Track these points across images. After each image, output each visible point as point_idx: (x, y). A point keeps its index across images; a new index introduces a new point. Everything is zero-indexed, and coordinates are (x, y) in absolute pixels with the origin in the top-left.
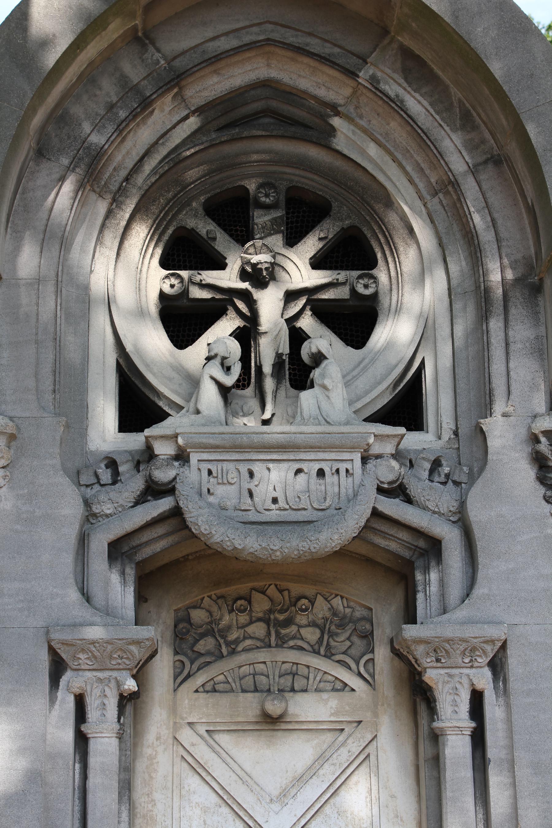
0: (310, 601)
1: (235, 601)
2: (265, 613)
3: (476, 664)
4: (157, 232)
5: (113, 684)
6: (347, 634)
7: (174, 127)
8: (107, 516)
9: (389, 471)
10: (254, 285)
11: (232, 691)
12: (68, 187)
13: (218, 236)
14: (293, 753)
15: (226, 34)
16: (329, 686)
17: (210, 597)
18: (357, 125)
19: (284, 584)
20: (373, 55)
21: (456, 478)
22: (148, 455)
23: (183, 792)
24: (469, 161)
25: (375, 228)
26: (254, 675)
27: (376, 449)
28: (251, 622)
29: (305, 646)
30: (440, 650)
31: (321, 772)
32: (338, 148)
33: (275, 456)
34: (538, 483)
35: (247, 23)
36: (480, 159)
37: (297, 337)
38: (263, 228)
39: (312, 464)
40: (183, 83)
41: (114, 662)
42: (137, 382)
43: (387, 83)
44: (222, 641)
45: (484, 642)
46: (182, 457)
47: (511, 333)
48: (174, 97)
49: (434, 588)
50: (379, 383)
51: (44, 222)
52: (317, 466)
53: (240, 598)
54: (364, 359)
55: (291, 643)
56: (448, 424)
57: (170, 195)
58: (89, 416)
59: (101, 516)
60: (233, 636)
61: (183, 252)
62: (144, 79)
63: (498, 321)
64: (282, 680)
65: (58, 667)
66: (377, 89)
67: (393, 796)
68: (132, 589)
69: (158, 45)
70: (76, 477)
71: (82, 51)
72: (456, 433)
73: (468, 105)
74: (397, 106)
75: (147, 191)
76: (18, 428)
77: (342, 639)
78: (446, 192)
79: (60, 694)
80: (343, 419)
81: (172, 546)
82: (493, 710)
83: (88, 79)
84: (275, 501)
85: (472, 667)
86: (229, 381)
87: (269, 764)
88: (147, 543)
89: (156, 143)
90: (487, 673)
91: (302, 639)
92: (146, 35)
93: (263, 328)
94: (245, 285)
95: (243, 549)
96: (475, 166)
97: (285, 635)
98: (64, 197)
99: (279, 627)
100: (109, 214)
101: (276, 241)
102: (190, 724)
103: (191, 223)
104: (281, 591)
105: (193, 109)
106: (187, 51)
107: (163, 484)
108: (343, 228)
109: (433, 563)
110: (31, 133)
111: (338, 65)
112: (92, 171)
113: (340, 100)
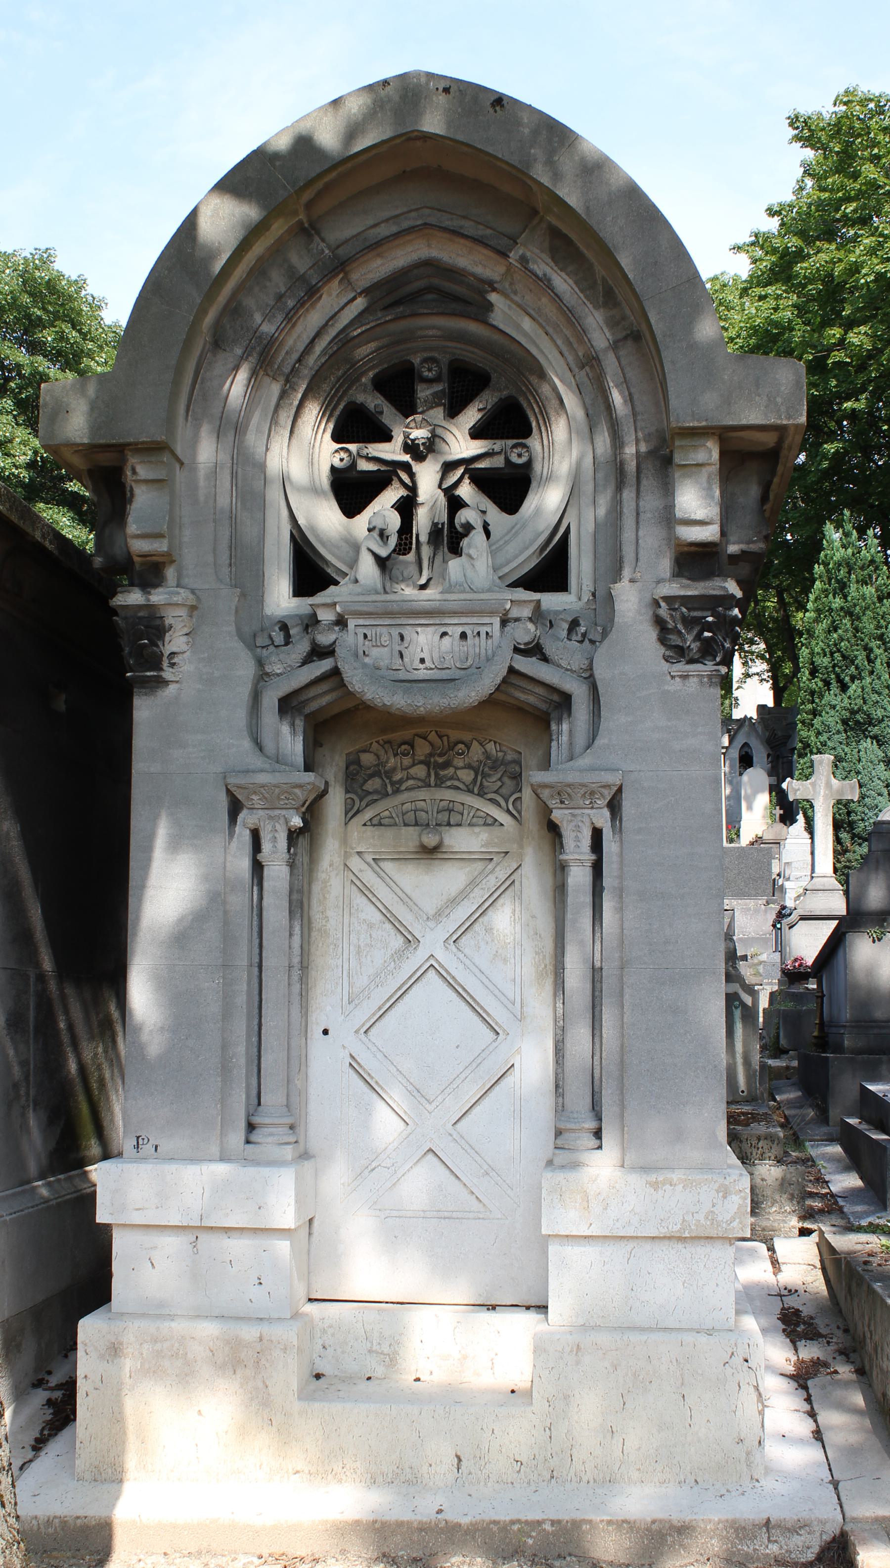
0: (466, 746)
1: (400, 746)
2: (426, 757)
3: (596, 806)
4: (327, 410)
5: (282, 821)
6: (499, 775)
7: (342, 308)
8: (278, 675)
9: (525, 633)
10: (413, 459)
11: (395, 825)
12: (242, 376)
13: (385, 409)
14: (448, 879)
15: (387, 220)
16: (481, 821)
17: (377, 742)
18: (512, 300)
19: (444, 731)
20: (523, 236)
21: (591, 637)
22: (311, 622)
23: (353, 911)
24: (610, 338)
25: (531, 398)
26: (415, 811)
27: (514, 613)
28: (414, 765)
29: (461, 786)
30: (562, 793)
31: (471, 895)
32: (495, 323)
33: (423, 621)
34: (659, 643)
35: (405, 209)
36: (620, 335)
37: (455, 504)
38: (425, 401)
39: (456, 628)
40: (347, 269)
41: (282, 803)
42: (308, 551)
43: (535, 262)
44: (387, 781)
45: (601, 787)
46: (341, 622)
47: (641, 503)
48: (340, 282)
49: (565, 738)
50: (527, 548)
51: (221, 409)
52: (460, 629)
53: (405, 743)
54: (516, 524)
55: (449, 783)
56: (588, 585)
57: (340, 373)
58: (265, 583)
59: (273, 675)
60: (398, 777)
61: (354, 426)
62: (310, 268)
63: (631, 492)
64: (440, 816)
65: (235, 808)
66: (525, 268)
67: (533, 917)
68: (301, 738)
69: (323, 235)
70: (251, 643)
71: (247, 252)
72: (594, 595)
73: (610, 282)
74: (545, 283)
75: (317, 371)
76: (198, 599)
77: (494, 780)
78: (589, 365)
79: (237, 829)
80: (487, 585)
81: (336, 700)
82: (610, 845)
83: (259, 271)
84: (422, 661)
85: (592, 808)
86: (383, 553)
87: (431, 886)
88: (314, 698)
89: (326, 324)
90: (606, 813)
91: (458, 780)
92: (312, 225)
93: (420, 499)
94: (407, 458)
95: (391, 705)
96: (615, 342)
97: (444, 776)
98: (237, 387)
99: (438, 770)
100: (284, 394)
101: (437, 414)
102: (359, 853)
103: (360, 398)
104: (440, 737)
105: (359, 291)
106: (349, 240)
107: (325, 647)
108: (501, 399)
109: (565, 716)
110: (205, 331)
111: (490, 246)
112: (264, 359)
113: (496, 277)
